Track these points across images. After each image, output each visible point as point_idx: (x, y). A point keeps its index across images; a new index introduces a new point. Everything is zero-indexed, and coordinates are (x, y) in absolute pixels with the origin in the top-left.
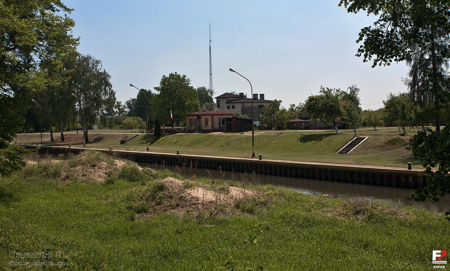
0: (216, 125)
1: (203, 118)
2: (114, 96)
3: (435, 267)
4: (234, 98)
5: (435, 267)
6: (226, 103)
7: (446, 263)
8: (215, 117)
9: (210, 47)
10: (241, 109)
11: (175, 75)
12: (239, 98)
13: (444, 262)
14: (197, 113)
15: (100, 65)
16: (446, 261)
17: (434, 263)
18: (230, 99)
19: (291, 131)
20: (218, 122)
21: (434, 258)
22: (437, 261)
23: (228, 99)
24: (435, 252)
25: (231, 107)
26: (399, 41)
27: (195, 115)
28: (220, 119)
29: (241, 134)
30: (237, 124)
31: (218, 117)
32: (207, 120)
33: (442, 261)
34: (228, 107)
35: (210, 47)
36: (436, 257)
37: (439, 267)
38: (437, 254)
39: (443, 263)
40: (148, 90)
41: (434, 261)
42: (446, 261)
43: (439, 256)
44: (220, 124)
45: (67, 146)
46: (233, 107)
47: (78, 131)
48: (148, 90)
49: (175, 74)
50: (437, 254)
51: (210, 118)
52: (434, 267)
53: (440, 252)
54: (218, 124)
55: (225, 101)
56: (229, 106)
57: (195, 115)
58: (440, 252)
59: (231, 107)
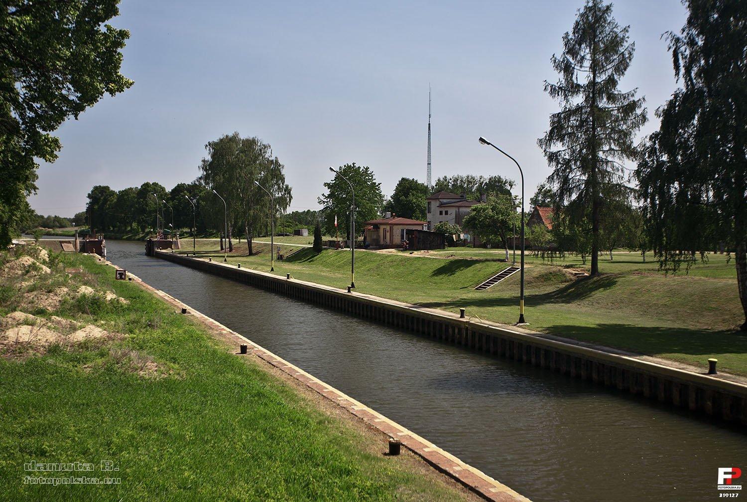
0: (397, 240)
1: (382, 227)
2: (289, 193)
3: (723, 495)
4: (451, 200)
5: (723, 495)
6: (438, 206)
7: (741, 489)
8: (395, 227)
9: (429, 124)
10: (454, 215)
11: (353, 168)
12: (459, 200)
13: (736, 486)
14: (374, 221)
15: (269, 151)
16: (741, 486)
17: (720, 489)
18: (445, 201)
19: (491, 252)
20: (400, 235)
21: (720, 481)
22: (726, 486)
23: (441, 200)
24: (721, 471)
25: (444, 213)
26: (724, 111)
27: (371, 224)
28: (403, 231)
29: (411, 253)
30: (419, 239)
31: (401, 227)
32: (385, 230)
33: (734, 486)
34: (441, 213)
35: (429, 124)
36: (724, 479)
37: (729, 495)
38: (725, 473)
39: (735, 489)
40: (88, 201)
41: (721, 485)
42: (741, 486)
43: (730, 476)
44: (402, 238)
45: (250, 266)
46: (446, 213)
47: (642, 261)
48: (88, 201)
49: (352, 166)
50: (725, 473)
51: (388, 228)
52: (721, 496)
53: (731, 471)
54: (400, 237)
55: (438, 203)
56: (442, 211)
57: (371, 224)
58: (730, 470)
59: (444, 213)
